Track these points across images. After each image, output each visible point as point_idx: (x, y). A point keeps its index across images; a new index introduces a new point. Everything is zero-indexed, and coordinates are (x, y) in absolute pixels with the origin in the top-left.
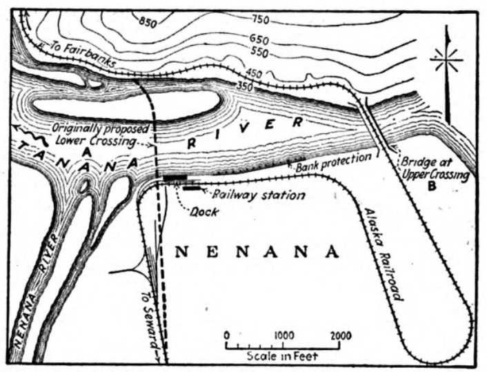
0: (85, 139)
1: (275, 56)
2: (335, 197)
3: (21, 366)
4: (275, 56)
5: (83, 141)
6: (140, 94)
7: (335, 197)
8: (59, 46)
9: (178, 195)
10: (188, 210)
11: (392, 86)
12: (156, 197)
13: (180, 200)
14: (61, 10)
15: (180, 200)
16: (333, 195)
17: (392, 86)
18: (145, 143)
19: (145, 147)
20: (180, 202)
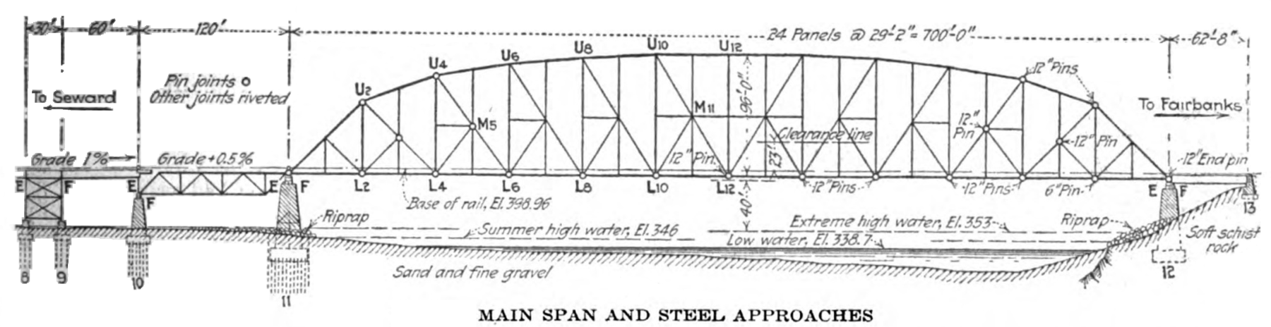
0: (541, 228)
1: (1248, 132)
2: (1169, 139)
3: (694, 179)
4: (1248, 132)
5: (540, 230)
6: (85, 164)
7: (1169, 139)
8: (1150, 103)
9: (1137, 38)
10: (1184, 39)
11: (965, 157)
12: (1171, 137)
13: (635, 34)
14: (473, 70)
15: (635, 34)
16: (1167, 136)
17: (965, 157)
18: (304, 35)
19: (305, 29)
20: (330, 32)
